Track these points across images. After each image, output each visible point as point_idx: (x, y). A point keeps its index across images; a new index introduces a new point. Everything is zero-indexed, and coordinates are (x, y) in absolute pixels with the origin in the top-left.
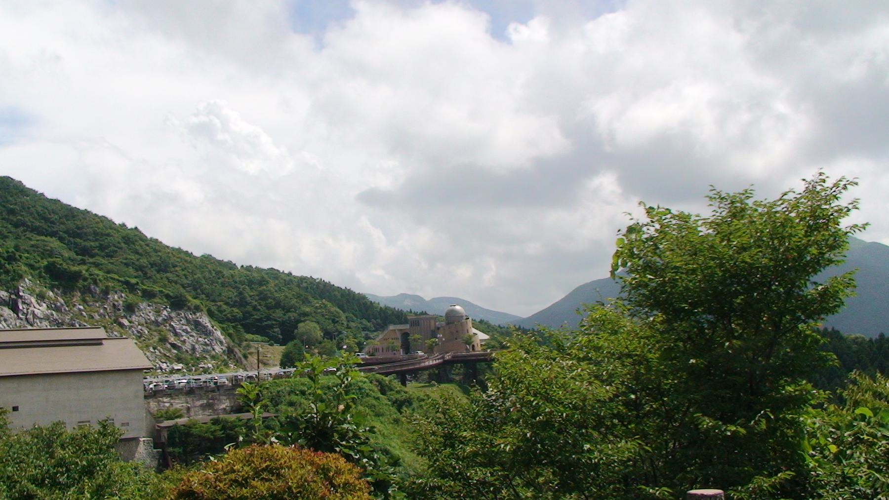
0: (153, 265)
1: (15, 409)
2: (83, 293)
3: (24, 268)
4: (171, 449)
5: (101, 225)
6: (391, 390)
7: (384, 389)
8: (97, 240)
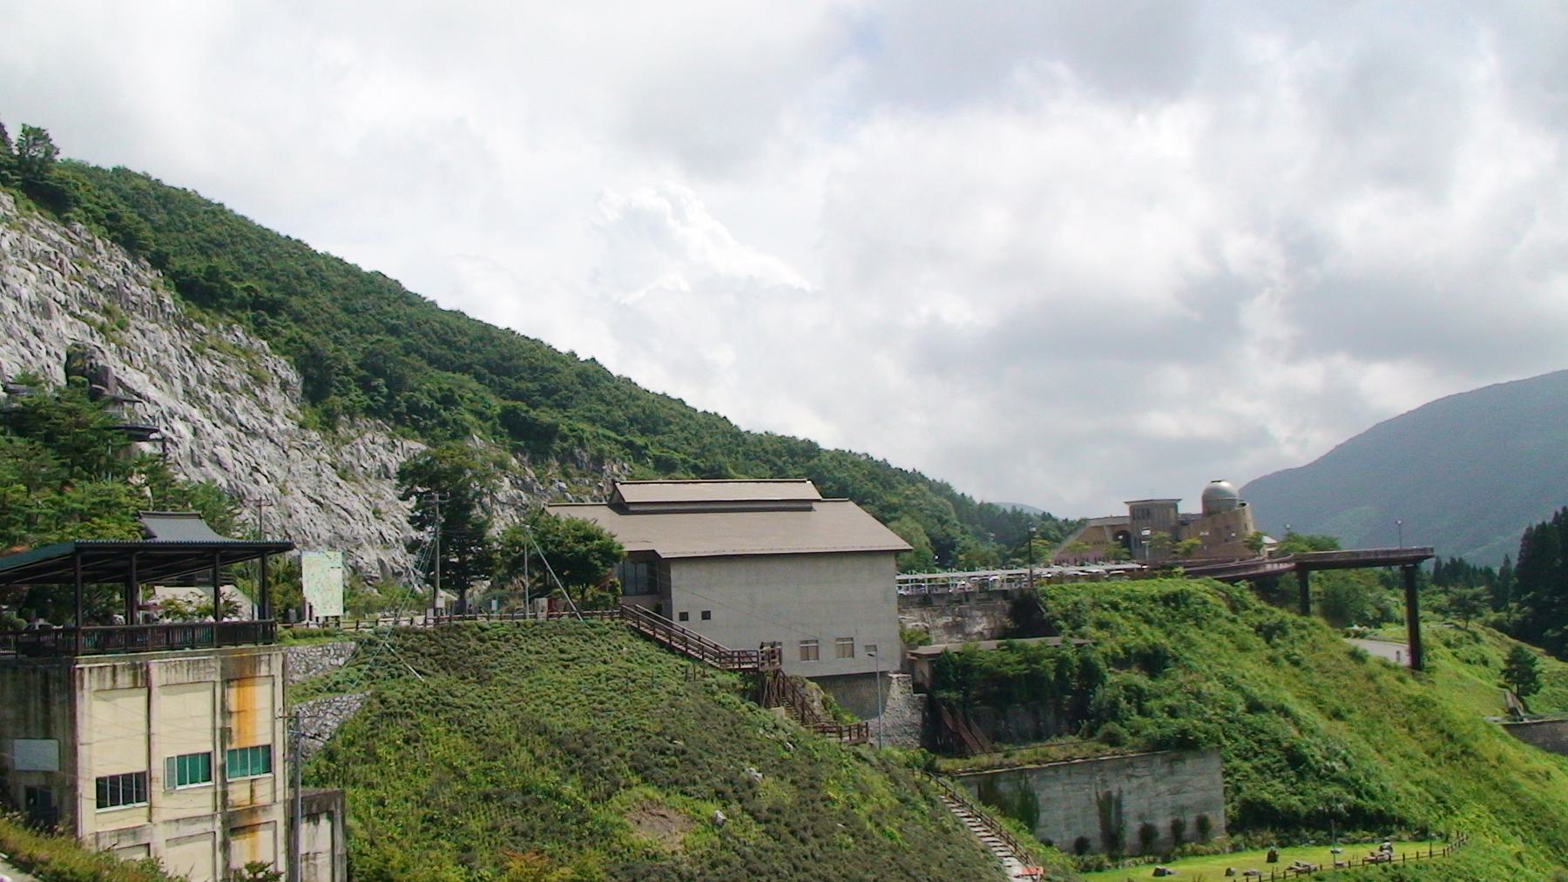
0: (633, 421)
1: (706, 615)
2: (562, 462)
3: (470, 417)
4: (945, 694)
5: (538, 354)
6: (1246, 608)
7: (1236, 606)
8: (535, 379)
